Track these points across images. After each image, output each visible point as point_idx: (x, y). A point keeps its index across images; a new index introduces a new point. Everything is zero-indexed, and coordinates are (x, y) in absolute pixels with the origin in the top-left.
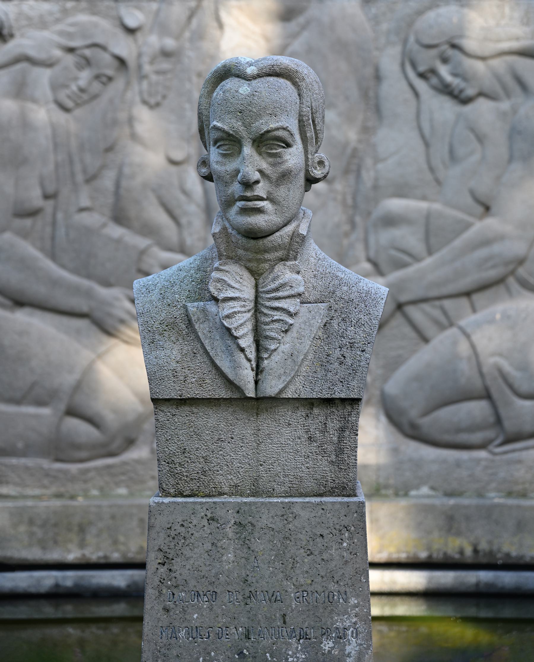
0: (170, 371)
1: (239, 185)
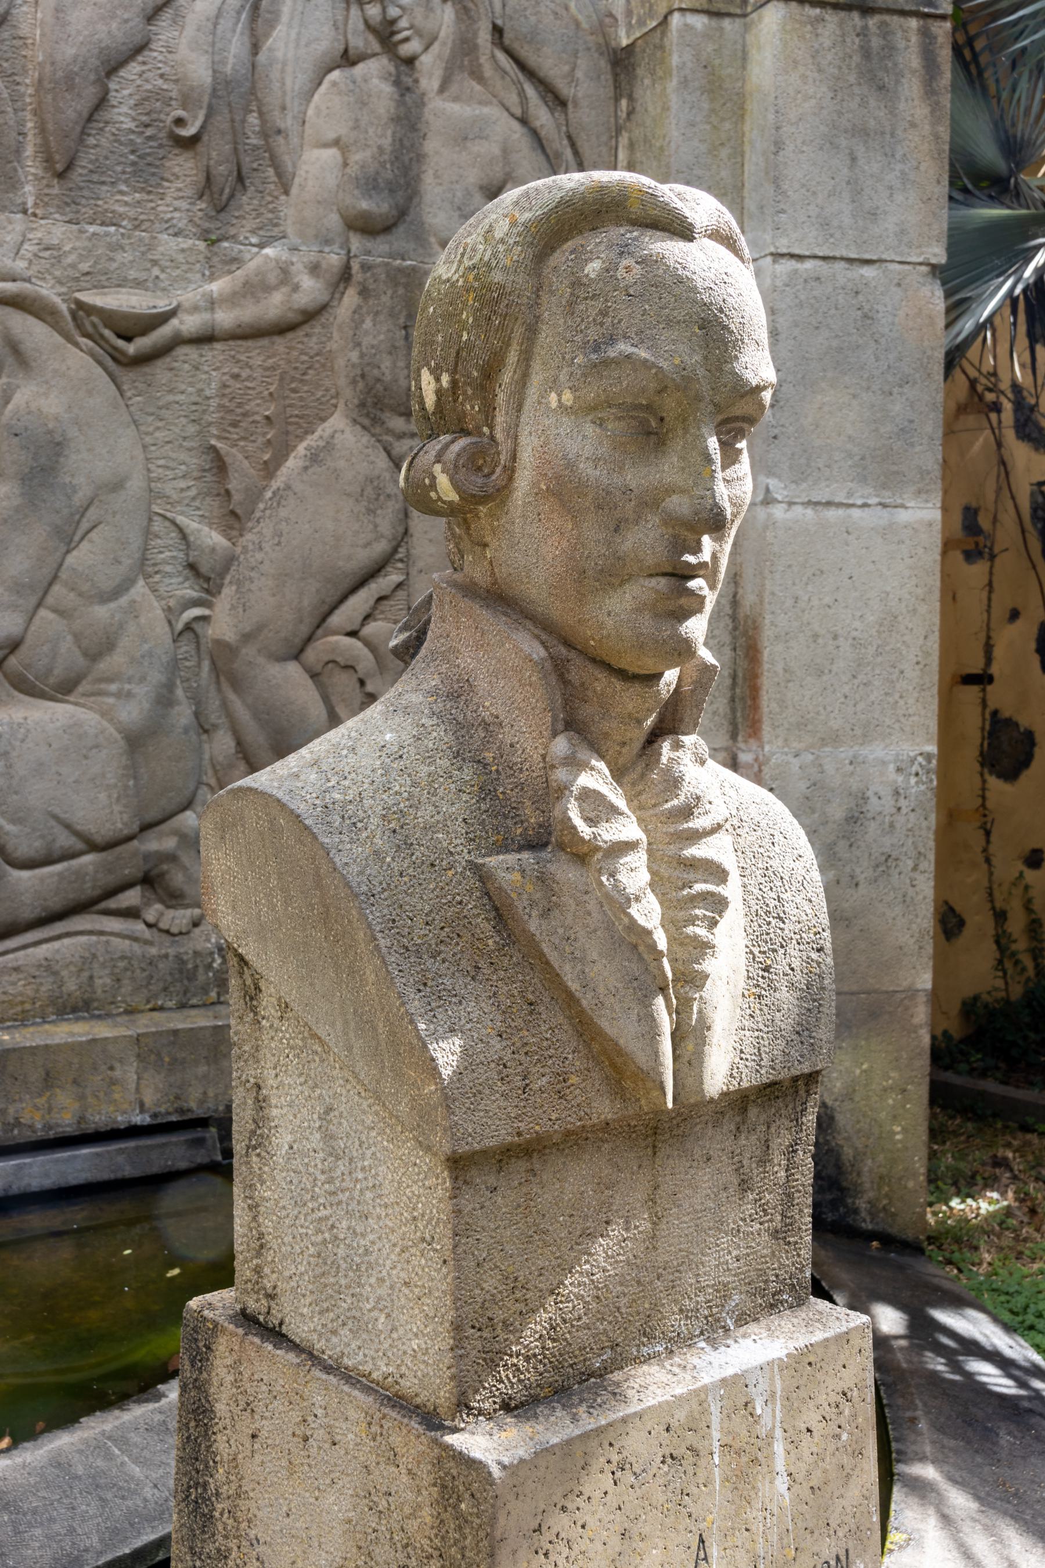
0: (493, 1065)
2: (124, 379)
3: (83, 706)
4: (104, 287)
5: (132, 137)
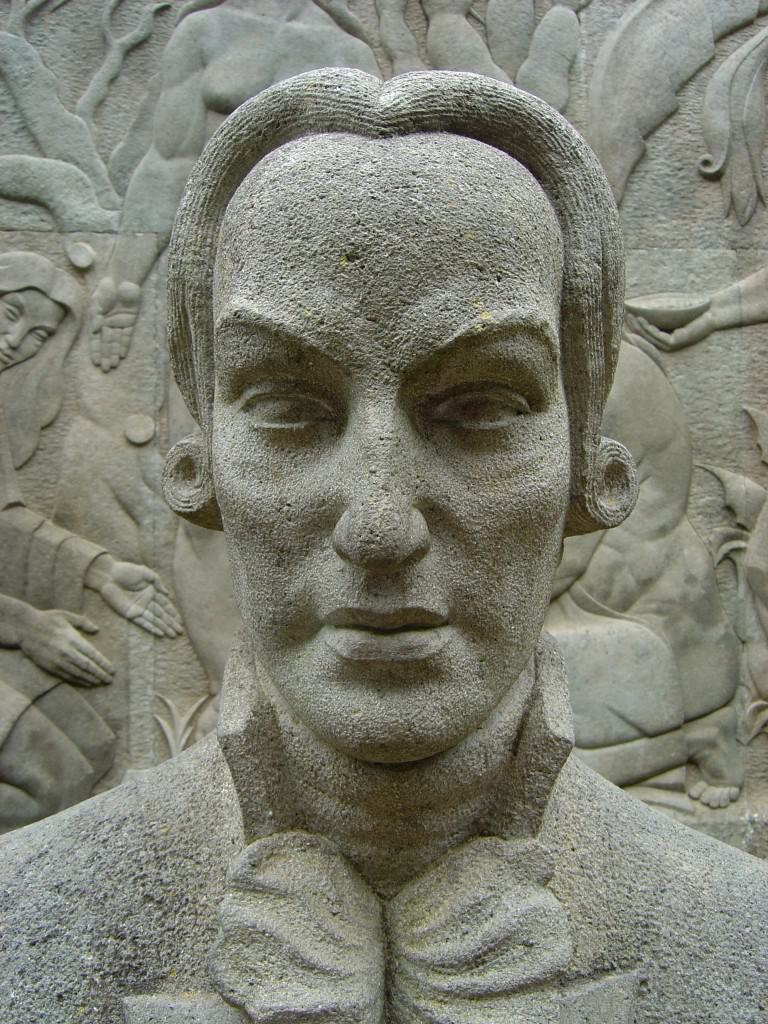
1: (340, 563)
2: (668, 363)
3: (636, 621)
4: (649, 294)
5: (668, 179)
